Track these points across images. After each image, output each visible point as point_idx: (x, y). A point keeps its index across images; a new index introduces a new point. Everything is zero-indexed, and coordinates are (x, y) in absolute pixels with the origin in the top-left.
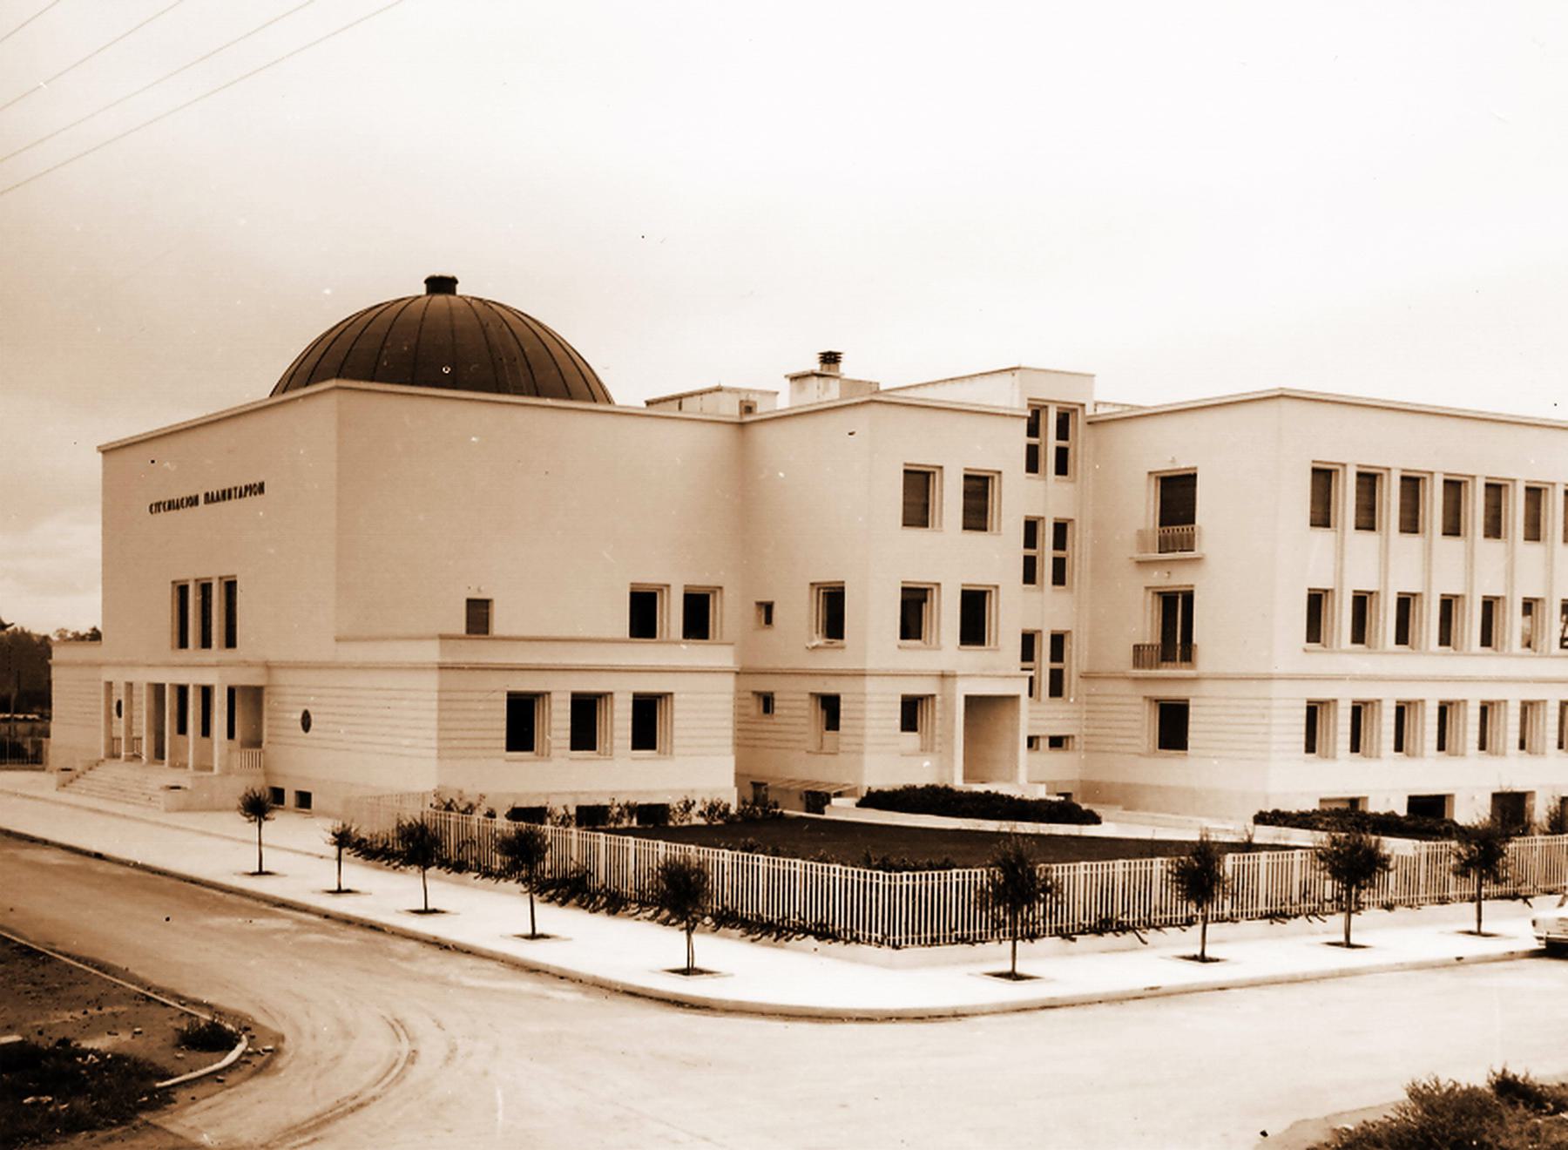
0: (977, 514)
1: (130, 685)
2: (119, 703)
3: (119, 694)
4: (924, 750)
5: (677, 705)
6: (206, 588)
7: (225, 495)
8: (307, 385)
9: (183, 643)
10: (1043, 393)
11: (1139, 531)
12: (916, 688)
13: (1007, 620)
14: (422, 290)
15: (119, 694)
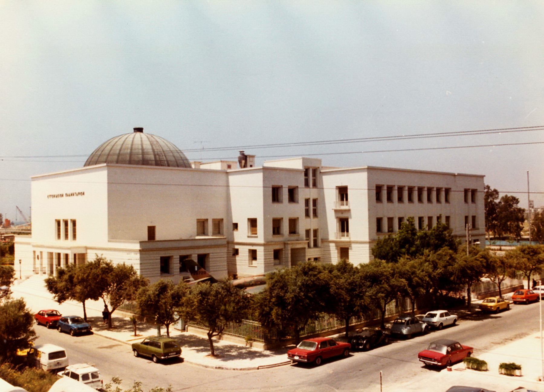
0: (292, 198)
1: (41, 252)
2: (38, 256)
3: (38, 253)
4: (280, 264)
5: (210, 257)
6: (66, 223)
7: (72, 195)
8: (96, 164)
9: (59, 236)
10: (309, 165)
11: (282, 186)
12: (277, 247)
13: (302, 228)
14: (234, 222)
15: (38, 253)
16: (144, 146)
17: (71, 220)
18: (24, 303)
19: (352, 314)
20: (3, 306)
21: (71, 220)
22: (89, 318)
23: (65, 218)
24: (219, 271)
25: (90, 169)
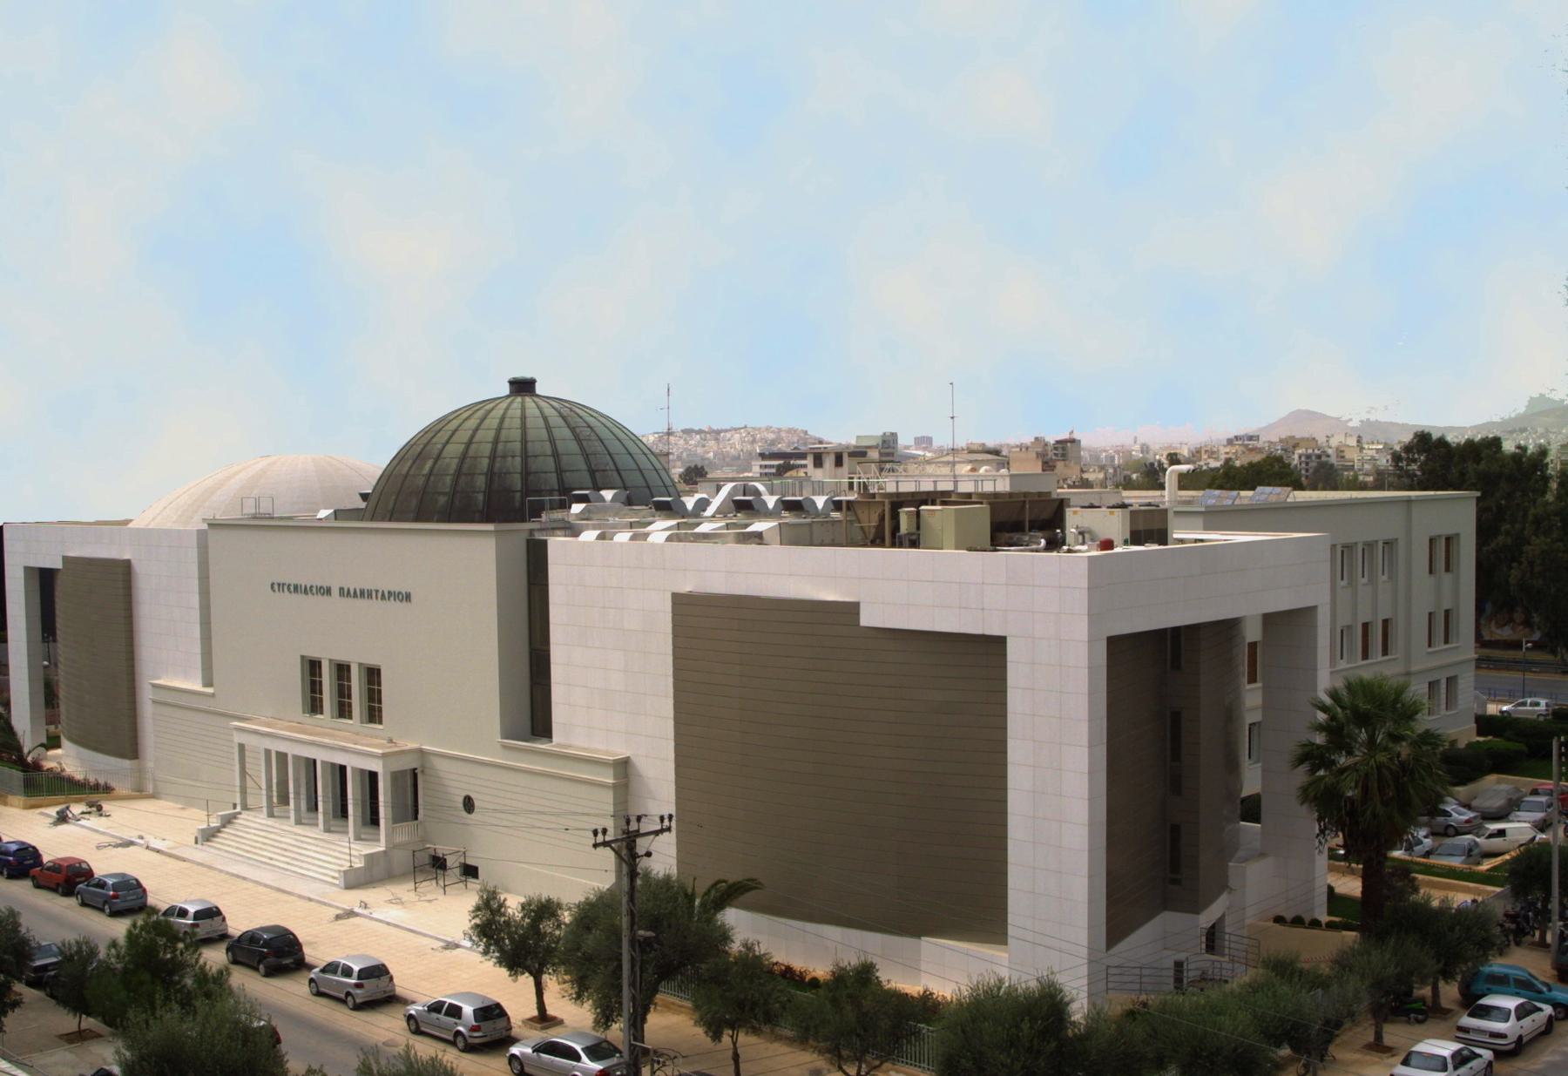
9: (315, 706)
16: (534, 465)
17: (331, 661)
18: (555, 900)
19: (1058, 531)
20: (661, 875)
21: (331, 661)
22: (1352, 872)
23: (342, 657)
24: (1392, 1034)
25: (427, 530)
